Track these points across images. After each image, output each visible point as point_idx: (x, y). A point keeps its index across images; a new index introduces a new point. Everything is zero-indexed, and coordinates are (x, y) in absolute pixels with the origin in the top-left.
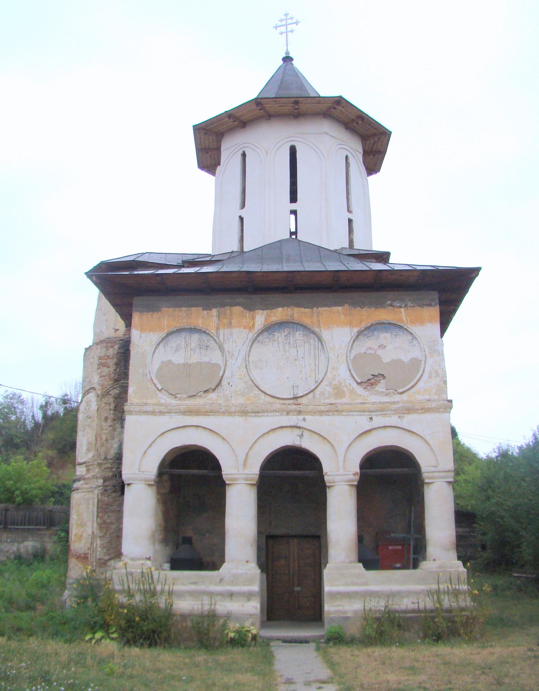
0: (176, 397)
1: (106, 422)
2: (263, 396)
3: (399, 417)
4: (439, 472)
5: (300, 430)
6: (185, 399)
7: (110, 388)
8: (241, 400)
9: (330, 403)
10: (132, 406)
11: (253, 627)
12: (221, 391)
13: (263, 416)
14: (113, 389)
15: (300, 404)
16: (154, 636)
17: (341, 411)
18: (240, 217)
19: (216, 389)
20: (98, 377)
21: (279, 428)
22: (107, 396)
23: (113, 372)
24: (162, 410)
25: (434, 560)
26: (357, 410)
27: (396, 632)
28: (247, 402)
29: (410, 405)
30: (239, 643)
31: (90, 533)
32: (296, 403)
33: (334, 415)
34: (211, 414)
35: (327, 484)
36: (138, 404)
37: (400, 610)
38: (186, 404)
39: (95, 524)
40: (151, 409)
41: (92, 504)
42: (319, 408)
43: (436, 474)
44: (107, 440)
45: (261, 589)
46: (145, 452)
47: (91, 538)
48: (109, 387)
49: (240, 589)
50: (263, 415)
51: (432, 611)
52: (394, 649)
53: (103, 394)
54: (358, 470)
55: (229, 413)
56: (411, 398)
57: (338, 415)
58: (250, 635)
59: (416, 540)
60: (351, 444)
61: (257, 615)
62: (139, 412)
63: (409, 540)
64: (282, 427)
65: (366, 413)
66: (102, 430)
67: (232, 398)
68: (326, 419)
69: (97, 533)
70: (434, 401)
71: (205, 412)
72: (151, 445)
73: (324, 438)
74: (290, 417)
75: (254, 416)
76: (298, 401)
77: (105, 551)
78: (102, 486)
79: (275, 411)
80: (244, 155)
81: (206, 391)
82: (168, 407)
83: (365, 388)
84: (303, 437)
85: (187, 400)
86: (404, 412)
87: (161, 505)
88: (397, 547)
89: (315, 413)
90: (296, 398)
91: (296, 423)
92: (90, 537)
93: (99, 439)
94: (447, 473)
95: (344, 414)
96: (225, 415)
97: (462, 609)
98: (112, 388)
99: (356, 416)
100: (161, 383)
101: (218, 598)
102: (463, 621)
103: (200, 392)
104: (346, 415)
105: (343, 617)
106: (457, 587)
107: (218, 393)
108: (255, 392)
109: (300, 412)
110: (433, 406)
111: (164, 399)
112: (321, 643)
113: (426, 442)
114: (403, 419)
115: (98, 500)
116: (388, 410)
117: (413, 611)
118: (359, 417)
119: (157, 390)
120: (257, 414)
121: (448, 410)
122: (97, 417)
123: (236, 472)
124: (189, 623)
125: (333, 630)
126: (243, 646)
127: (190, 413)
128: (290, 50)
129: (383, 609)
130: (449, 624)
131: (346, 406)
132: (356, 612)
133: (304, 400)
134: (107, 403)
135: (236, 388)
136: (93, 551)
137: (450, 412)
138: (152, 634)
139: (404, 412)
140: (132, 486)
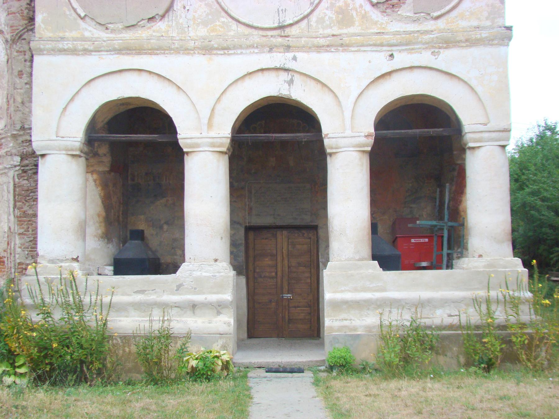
0: (107, 29)
1: (21, 78)
2: (234, 25)
3: (432, 52)
4: (490, 131)
5: (288, 75)
6: (120, 31)
7: (22, 30)
8: (202, 32)
9: (332, 34)
10: (42, 42)
11: (225, 352)
12: (174, 18)
13: (234, 54)
14: (28, 31)
15: (288, 36)
16: (82, 367)
17: (348, 46)
19: (167, 16)
20: (5, 14)
21: (258, 71)
22: (20, 42)
23: (26, 6)
24: (86, 47)
25: (480, 256)
26: (371, 43)
27: (428, 357)
28: (211, 34)
29: (450, 35)
30: (203, 374)
31: (6, 229)
32: (283, 34)
33: (337, 51)
34: (158, 52)
35: (328, 151)
36: (51, 39)
37: (433, 326)
38: (121, 37)
39: (12, 217)
40: (71, 46)
41: (6, 191)
42: (316, 41)
43: (486, 135)
44: (23, 103)
45: (237, 299)
46: (65, 109)
47: (8, 236)
48: (22, 28)
49: (206, 299)
50: (235, 53)
51: (477, 327)
52: (429, 385)
53: (13, 38)
54: (372, 130)
55: (186, 51)
56: (450, 24)
57: (343, 51)
58: (220, 363)
59: (451, 230)
60: (362, 93)
61: (230, 334)
62: (53, 50)
63: (442, 229)
64: (262, 70)
65: (385, 48)
66: (15, 88)
67: (190, 29)
68: (326, 56)
69: (14, 229)
70: (484, 28)
71: (150, 50)
72: (72, 99)
73: (324, 85)
74: (275, 54)
75: (221, 54)
76: (286, 32)
77: (27, 253)
78: (19, 165)
79: (252, 46)
81: (151, 19)
82: (96, 43)
83: (385, 12)
84: (293, 84)
85: (124, 32)
86: (441, 45)
87: (100, 188)
88: (422, 240)
89: (310, 48)
90: (282, 27)
91: (283, 64)
92: (7, 235)
93: (11, 102)
94: (501, 134)
95: (353, 49)
96: (179, 53)
97: (523, 326)
98: (26, 30)
99: (369, 53)
100: (84, 8)
101: (175, 311)
102: (524, 342)
103: (143, 19)
104: (356, 51)
105: (351, 336)
106: (516, 294)
107: (168, 22)
108: (223, 20)
109: (288, 48)
110: (483, 36)
111: (90, 31)
112: (320, 371)
113: (472, 89)
114: (439, 55)
115: (15, 184)
116: (417, 43)
117: (451, 327)
118: (374, 53)
119: (79, 18)
120: (226, 51)
121: (506, 41)
122: (8, 71)
123: (198, 135)
124: (134, 349)
125: (338, 354)
126: (208, 379)
127: (128, 52)
129: (408, 324)
130: (503, 346)
131: (355, 37)
132: (369, 328)
133: (294, 31)
134: (21, 52)
135: (194, 14)
136: (11, 254)
137: (508, 45)
138: (79, 366)
139: (441, 45)
140: (48, 158)
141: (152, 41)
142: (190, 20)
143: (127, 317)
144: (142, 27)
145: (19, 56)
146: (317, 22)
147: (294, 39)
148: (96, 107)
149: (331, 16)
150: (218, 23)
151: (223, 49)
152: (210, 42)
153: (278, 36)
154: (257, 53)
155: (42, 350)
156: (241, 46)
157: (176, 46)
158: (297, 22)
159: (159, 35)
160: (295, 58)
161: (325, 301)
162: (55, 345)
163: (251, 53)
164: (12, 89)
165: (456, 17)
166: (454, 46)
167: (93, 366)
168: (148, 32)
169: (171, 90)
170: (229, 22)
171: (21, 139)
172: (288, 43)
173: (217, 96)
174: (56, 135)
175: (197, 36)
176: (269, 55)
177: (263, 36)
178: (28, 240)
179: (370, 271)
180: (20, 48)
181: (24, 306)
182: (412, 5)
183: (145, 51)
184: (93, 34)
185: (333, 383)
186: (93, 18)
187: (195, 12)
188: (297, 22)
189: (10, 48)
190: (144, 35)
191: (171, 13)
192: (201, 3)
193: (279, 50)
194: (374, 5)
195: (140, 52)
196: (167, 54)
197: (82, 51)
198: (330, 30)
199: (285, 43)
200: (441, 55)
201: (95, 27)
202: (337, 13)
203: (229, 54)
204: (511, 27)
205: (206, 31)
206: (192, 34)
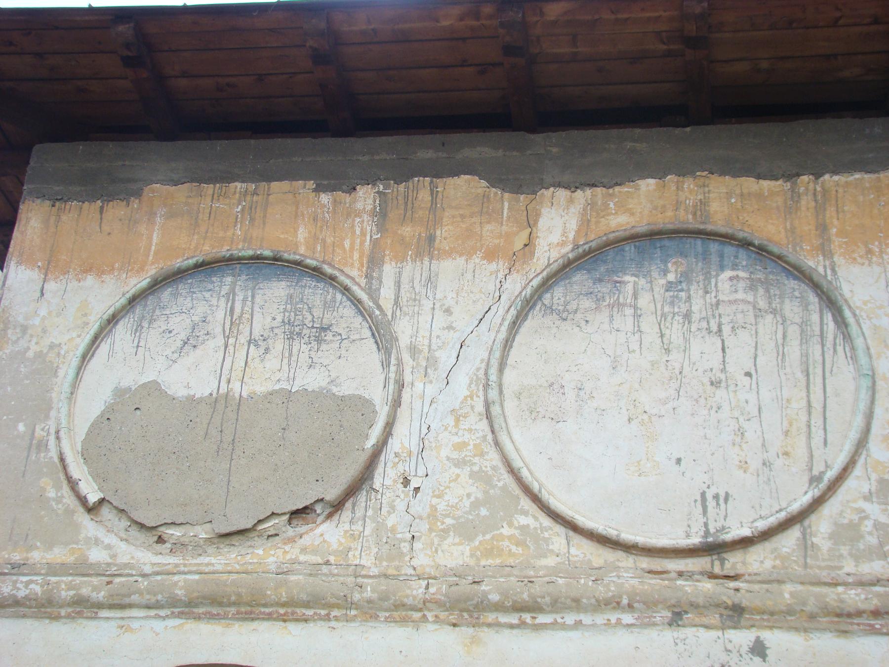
0: (160, 540)
2: (558, 537)
6: (199, 548)
12: (370, 513)
13: (554, 625)
15: (735, 578)
19: (348, 505)
24: (85, 591)
32: (717, 570)
34: (310, 612)
38: (199, 565)
40: (38, 589)
42: (832, 595)
50: (555, 623)
67: (417, 545)
71: (283, 605)
74: (689, 632)
75: (512, 626)
76: (728, 565)
79: (613, 603)
81: (300, 514)
82: (118, 580)
85: (211, 550)
89: (812, 617)
96: (376, 617)
108: (523, 520)
119: (81, 510)
120: (527, 617)
127: (215, 611)
135: (435, 501)
141: (293, 578)
142: (421, 518)
144: (269, 536)
146: (834, 537)
147: (756, 587)
150: (506, 531)
151: (519, 608)
152: (475, 586)
153: (702, 573)
154: (629, 626)
155: (316, 618)
156: (577, 601)
157: (368, 593)
158: (766, 535)
163: (608, 624)
167: (466, 456)
168: (285, 552)
170: (546, 529)
172: (737, 598)
175: (438, 567)
176: (669, 635)
183: (267, 610)
184: (114, 556)
186: (122, 507)
187: (439, 497)
188: (766, 535)
191: (362, 497)
192: (457, 471)
193: (705, 620)
195: (251, 613)
196: (336, 618)
197: (69, 605)
198: (882, 563)
199: (725, 598)
201: (125, 537)
205: (467, 553)
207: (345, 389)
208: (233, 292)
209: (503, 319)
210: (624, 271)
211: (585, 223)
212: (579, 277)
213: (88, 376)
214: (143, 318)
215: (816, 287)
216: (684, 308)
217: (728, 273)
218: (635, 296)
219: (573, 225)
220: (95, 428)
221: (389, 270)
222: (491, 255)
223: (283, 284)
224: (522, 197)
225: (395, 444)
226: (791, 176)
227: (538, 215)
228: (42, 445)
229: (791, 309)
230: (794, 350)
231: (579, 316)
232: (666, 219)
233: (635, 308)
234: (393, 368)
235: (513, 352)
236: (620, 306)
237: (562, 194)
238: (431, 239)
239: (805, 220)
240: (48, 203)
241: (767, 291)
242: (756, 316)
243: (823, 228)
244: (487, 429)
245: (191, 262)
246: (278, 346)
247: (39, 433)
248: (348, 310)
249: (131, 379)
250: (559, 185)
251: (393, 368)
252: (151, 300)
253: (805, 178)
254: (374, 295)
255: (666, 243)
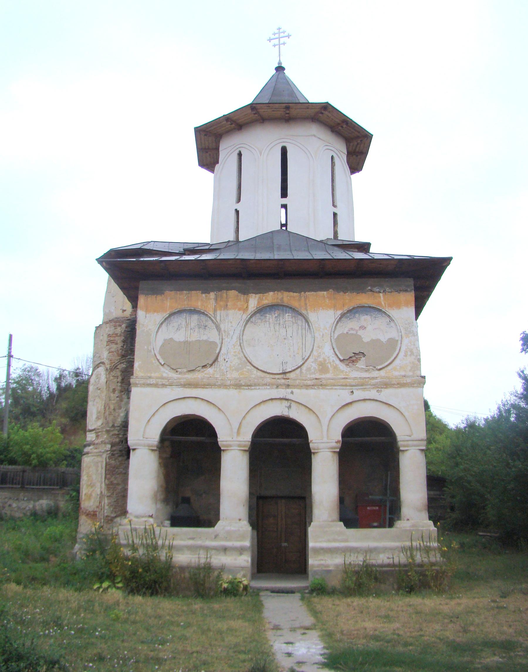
0: (177, 372)
1: (114, 393)
2: (255, 371)
3: (377, 391)
6: (185, 373)
7: (118, 363)
8: (235, 375)
11: (245, 579)
12: (218, 366)
13: (255, 389)
14: (121, 363)
17: (326, 385)
18: (236, 210)
19: (213, 364)
22: (115, 370)
24: (164, 382)
25: (408, 520)
26: (340, 384)
27: (373, 584)
28: (241, 377)
29: (388, 380)
32: (285, 377)
33: (319, 388)
34: (208, 387)
35: (312, 451)
36: (143, 378)
38: (185, 377)
39: (103, 485)
41: (100, 467)
42: (305, 382)
43: (410, 443)
44: (114, 409)
45: (252, 545)
46: (149, 421)
50: (255, 388)
51: (405, 566)
53: (111, 367)
54: (340, 439)
58: (242, 586)
60: (333, 415)
61: (248, 568)
62: (144, 384)
63: (386, 501)
64: (272, 399)
65: (348, 387)
66: (110, 400)
67: (228, 373)
68: (312, 392)
69: (104, 493)
70: (408, 377)
71: (203, 385)
72: (154, 414)
73: (310, 409)
74: (280, 390)
75: (247, 389)
76: (287, 376)
77: (112, 509)
78: (109, 451)
79: (266, 385)
80: (240, 155)
81: (204, 366)
82: (170, 380)
87: (163, 468)
89: (302, 386)
90: (284, 373)
92: (99, 497)
93: (107, 408)
95: (328, 387)
96: (221, 387)
97: (433, 564)
101: (213, 552)
103: (199, 367)
104: (330, 389)
105: (325, 571)
106: (428, 544)
108: (248, 367)
109: (288, 386)
112: (305, 593)
114: (381, 392)
115: (106, 463)
117: (389, 565)
118: (341, 390)
119: (160, 365)
120: (250, 387)
123: (231, 439)
125: (316, 581)
126: (235, 595)
127: (189, 386)
128: (282, 61)
129: (361, 563)
130: (421, 577)
132: (337, 566)
133: (292, 375)
134: (115, 377)
135: (231, 364)
136: (101, 509)
139: (382, 386)
140: (137, 451)
143: (182, 554)
145: (114, 379)
147: (292, 381)
148: (168, 420)
149: (315, 366)
150: (245, 370)
156: (259, 384)
157: (219, 383)
159: (208, 376)
160: (292, 393)
161: (309, 548)
162: (140, 570)
164: (108, 400)
165: (392, 369)
166: (390, 387)
169: (215, 410)
171: (112, 433)
173: (244, 415)
174: (143, 436)
177: (273, 378)
178: (113, 500)
179: (338, 529)
180: (115, 374)
181: (121, 545)
182: (365, 361)
185: (313, 599)
187: (232, 363)
189: (109, 373)
190: (199, 376)
191: (216, 363)
193: (283, 387)
194: (341, 361)
200: (382, 392)
202: (320, 365)
203: (252, 389)
204: (425, 376)
206: (228, 376)
207: (211, 340)
208: (186, 317)
209: (243, 324)
210: (266, 313)
211: (258, 302)
212: (258, 315)
213: (158, 336)
214: (168, 323)
215: (304, 317)
216: (279, 322)
217: (287, 314)
218: (269, 319)
219: (256, 303)
220: (161, 347)
221: (218, 312)
222: (239, 309)
223: (196, 316)
224: (245, 296)
225: (222, 352)
226: (300, 292)
227: (249, 300)
228: (150, 351)
229: (299, 322)
230: (300, 331)
231: (258, 324)
232: (275, 302)
233: (269, 322)
234: (221, 336)
235: (245, 332)
236: (266, 321)
237: (254, 295)
238: (227, 305)
239: (303, 302)
240: (145, 295)
241: (295, 318)
242: (293, 324)
243: (306, 304)
244: (240, 348)
245: (177, 310)
246: (197, 330)
247: (149, 349)
248: (210, 322)
249: (167, 337)
250: (253, 293)
251: (221, 336)
252: (169, 319)
253: (302, 293)
254: (215, 318)
255: (275, 307)
